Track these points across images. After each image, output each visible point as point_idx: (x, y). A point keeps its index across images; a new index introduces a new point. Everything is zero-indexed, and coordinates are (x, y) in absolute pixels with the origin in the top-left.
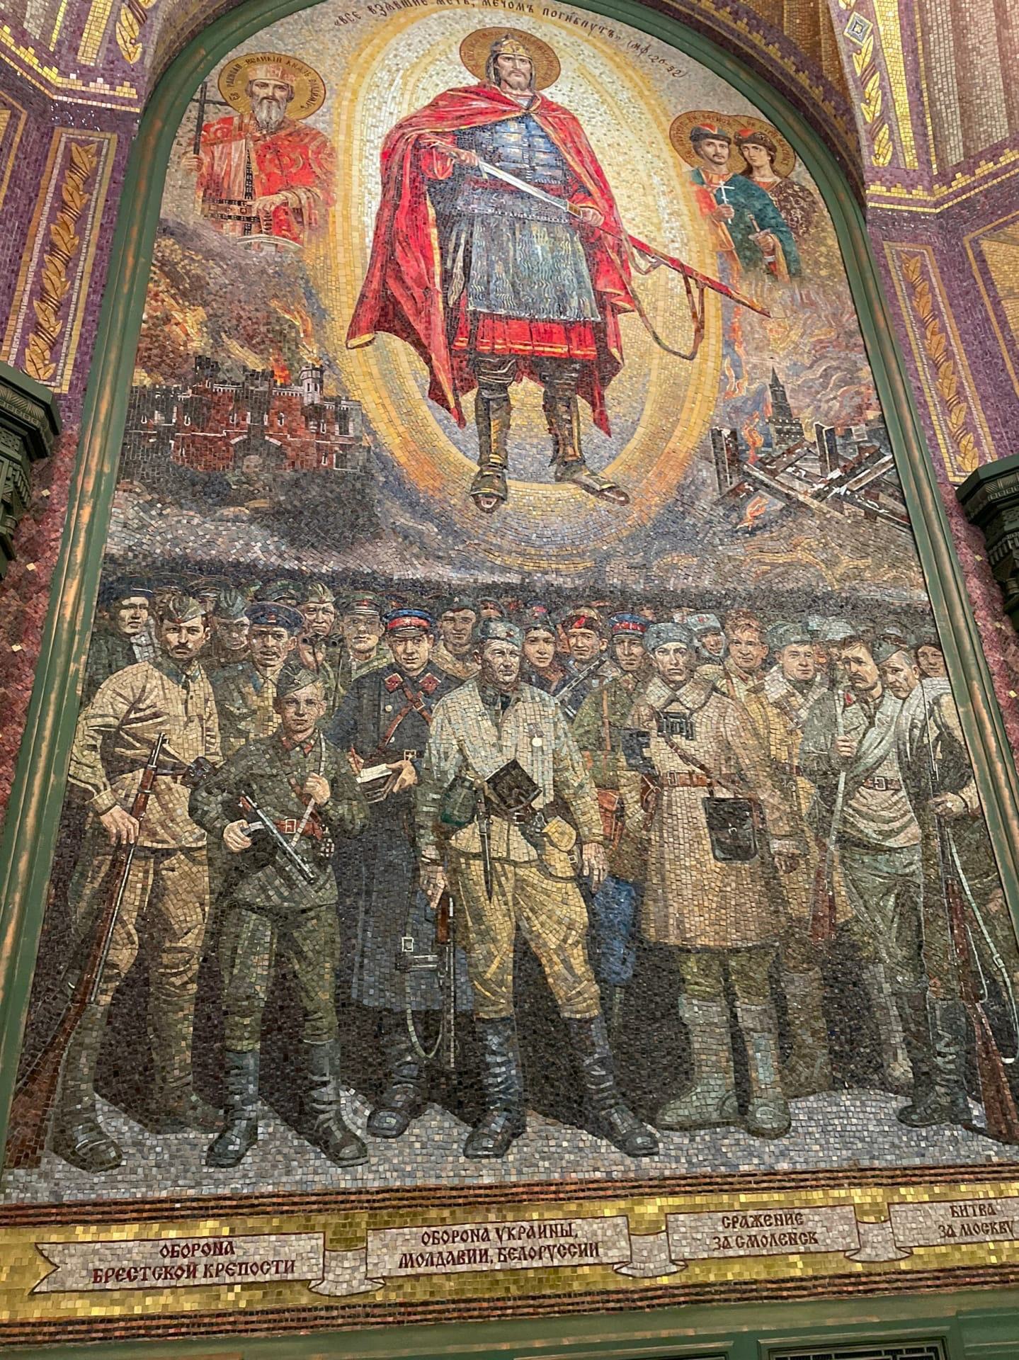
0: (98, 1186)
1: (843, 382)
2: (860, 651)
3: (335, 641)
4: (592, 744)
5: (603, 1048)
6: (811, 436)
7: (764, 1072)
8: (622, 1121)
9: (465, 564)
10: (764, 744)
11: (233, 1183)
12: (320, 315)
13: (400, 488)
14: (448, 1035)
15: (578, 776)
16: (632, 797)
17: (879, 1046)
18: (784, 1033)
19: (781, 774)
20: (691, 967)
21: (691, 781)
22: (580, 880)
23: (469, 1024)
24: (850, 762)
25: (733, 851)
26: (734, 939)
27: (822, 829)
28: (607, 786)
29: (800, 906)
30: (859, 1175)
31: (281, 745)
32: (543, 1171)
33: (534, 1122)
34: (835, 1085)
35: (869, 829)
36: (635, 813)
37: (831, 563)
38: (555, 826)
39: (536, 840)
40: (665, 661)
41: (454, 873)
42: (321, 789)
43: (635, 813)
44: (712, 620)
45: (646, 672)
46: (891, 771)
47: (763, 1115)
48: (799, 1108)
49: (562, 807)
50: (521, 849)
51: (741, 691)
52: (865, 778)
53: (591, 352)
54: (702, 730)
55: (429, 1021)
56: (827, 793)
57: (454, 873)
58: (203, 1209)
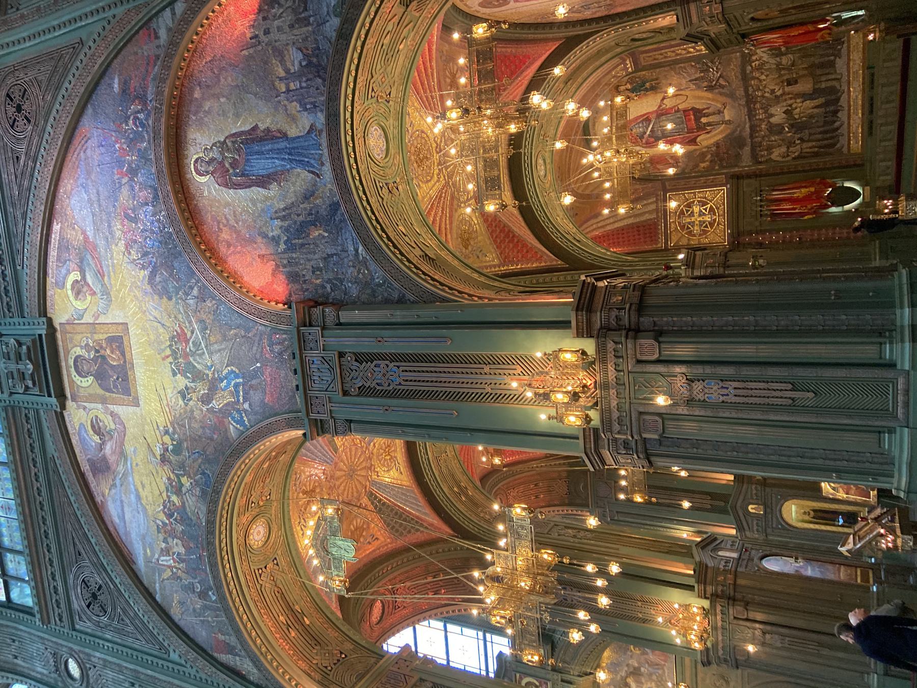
0: (846, 147)
1: (685, 69)
2: (753, 64)
3: (763, 137)
4: (778, 103)
5: (829, 97)
6: (702, 74)
7: (833, 77)
8: (840, 94)
9: (745, 123)
10: (774, 79)
11: (846, 134)
12: (695, 150)
13: (734, 132)
14: (827, 115)
15: (785, 104)
16: (787, 97)
17: (829, 61)
18: (828, 74)
19: (781, 76)
20: (817, 87)
21: (783, 89)
22: (803, 102)
23: (826, 113)
24: (777, 66)
25: (796, 82)
26: (812, 81)
27: (791, 69)
28: (786, 100)
29: (806, 72)
30: (848, 64)
31: (783, 140)
32: (846, 102)
33: (839, 104)
34: (835, 67)
35: (790, 63)
36: (790, 96)
37: (733, 70)
38: (794, 106)
39: (796, 108)
40: (760, 94)
41: (803, 117)
42: (789, 134)
43: (790, 96)
44: (750, 88)
45: (763, 96)
46: (778, 59)
47: (839, 77)
48: (838, 72)
49: (790, 106)
50: (798, 110)
51: (764, 82)
52: (780, 63)
53: (691, 112)
54: (773, 88)
55: (825, 117)
56: (783, 69)
57: (803, 117)
58: (849, 137)
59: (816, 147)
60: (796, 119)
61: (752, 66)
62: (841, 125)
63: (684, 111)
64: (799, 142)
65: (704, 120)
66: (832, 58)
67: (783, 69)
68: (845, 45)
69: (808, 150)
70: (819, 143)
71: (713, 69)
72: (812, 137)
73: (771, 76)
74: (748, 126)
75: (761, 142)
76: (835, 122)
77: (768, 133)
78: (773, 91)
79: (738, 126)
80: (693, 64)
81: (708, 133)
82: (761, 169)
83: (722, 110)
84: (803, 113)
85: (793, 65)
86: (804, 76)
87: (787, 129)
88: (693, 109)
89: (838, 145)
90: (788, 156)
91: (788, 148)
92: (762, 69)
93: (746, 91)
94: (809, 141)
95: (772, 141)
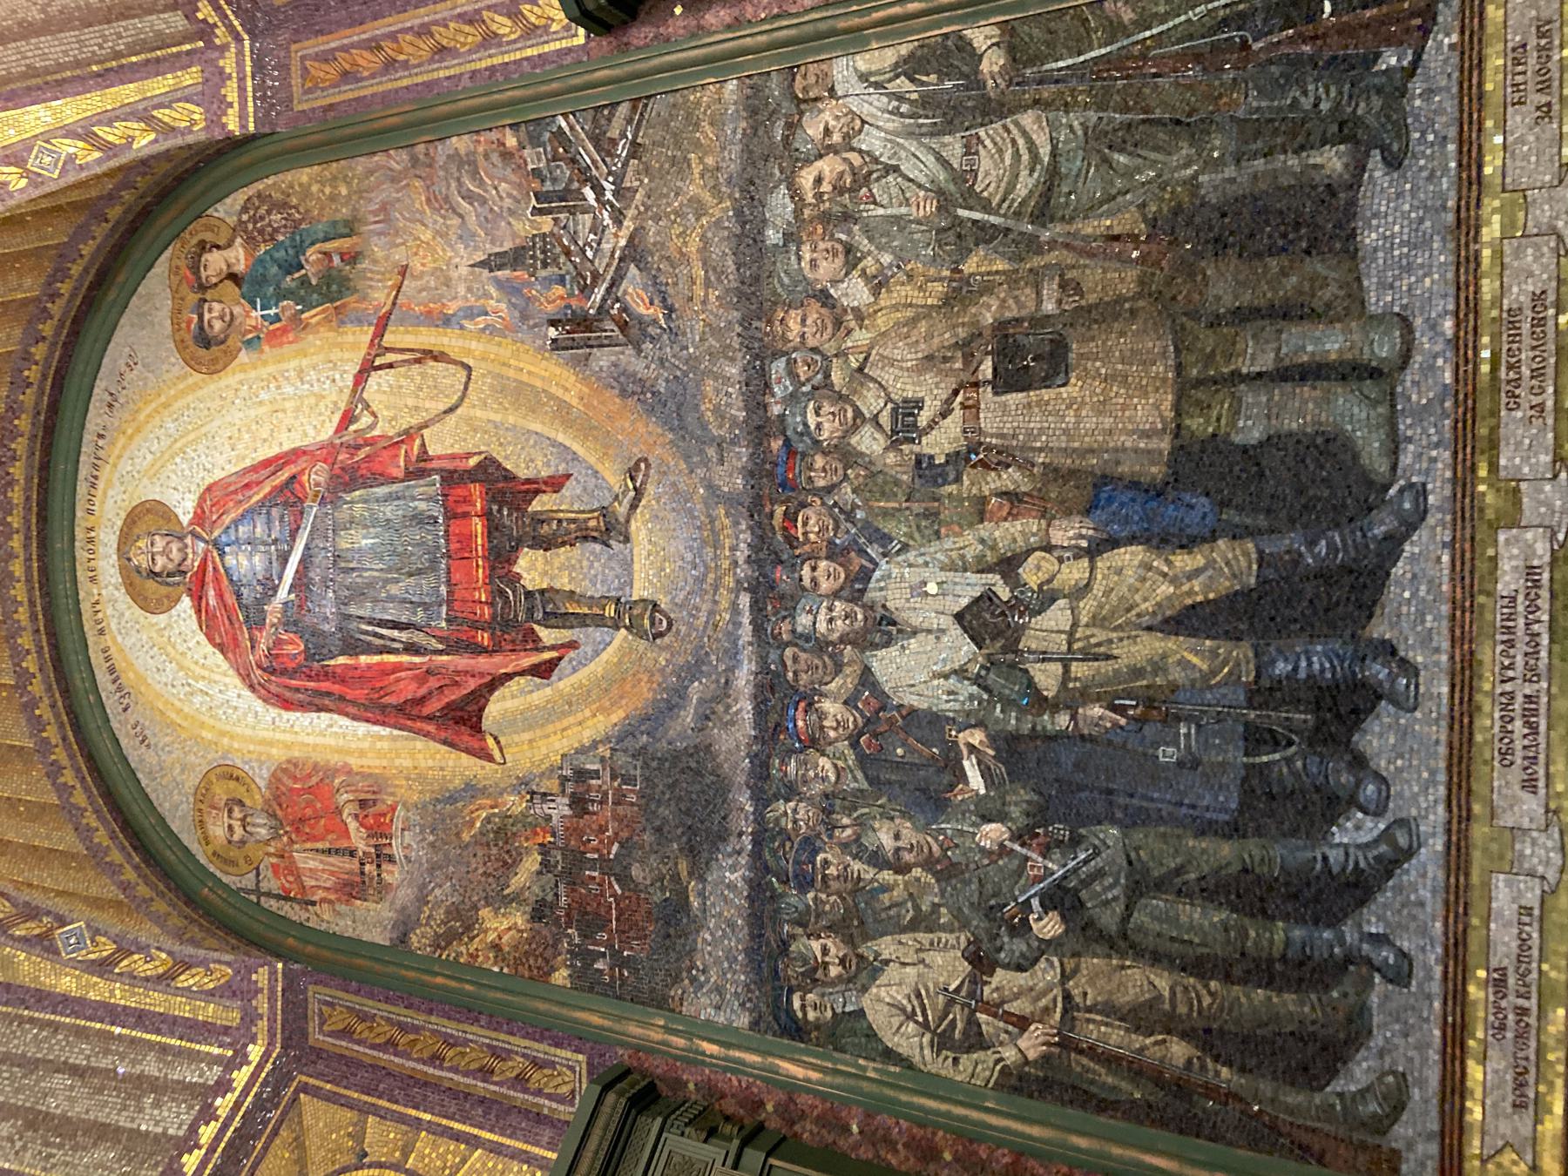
3: (829, 804)
4: (932, 523)
5: (1292, 540)
7: (1332, 343)
12: (472, 790)
14: (1275, 718)
15: (969, 542)
16: (995, 482)
17: (1305, 185)
21: (972, 408)
22: (1093, 551)
24: (945, 202)
27: (1032, 245)
28: (980, 509)
30: (1466, 227)
31: (946, 871)
32: (1437, 622)
33: (1379, 629)
36: (1011, 478)
38: (1032, 573)
39: (1047, 597)
42: (992, 833)
43: (1011, 478)
44: (778, 367)
45: (845, 455)
46: (953, 147)
47: (1383, 348)
48: (1377, 301)
49: (1008, 565)
50: (1057, 616)
53: (476, 490)
55: (1257, 738)
56: (985, 234)
59: (1171, 1025)
60: (1040, 703)
61: (795, 194)
62: (1393, 860)
63: (452, 478)
64: (1049, 926)
65: (532, 568)
66: (1332, 160)
67: (985, 234)
68: (1445, 39)
69: (1115, 1037)
70: (1208, 994)
71: (599, 190)
72: (1151, 914)
73: (901, 292)
74: (744, 676)
75: (811, 845)
76: (1335, 805)
77: (857, 781)
78: (905, 411)
79: (694, 670)
80: (511, 141)
81: (544, 671)
82: (792, 1088)
83: (622, 510)
84: (1089, 656)
85: (1043, 210)
86: (1105, 314)
87: (976, 781)
88: (489, 472)
89: (1360, 1072)
90: (976, 1041)
91: (981, 962)
92: (847, 217)
93: (757, 386)
94: (1123, 943)
95: (877, 859)
